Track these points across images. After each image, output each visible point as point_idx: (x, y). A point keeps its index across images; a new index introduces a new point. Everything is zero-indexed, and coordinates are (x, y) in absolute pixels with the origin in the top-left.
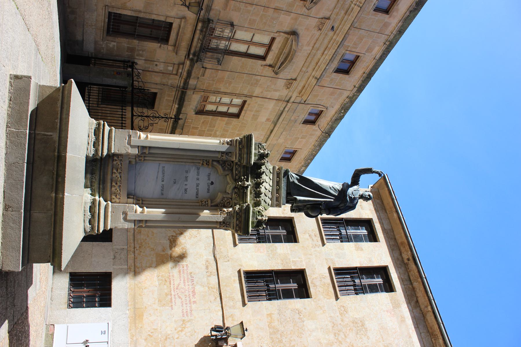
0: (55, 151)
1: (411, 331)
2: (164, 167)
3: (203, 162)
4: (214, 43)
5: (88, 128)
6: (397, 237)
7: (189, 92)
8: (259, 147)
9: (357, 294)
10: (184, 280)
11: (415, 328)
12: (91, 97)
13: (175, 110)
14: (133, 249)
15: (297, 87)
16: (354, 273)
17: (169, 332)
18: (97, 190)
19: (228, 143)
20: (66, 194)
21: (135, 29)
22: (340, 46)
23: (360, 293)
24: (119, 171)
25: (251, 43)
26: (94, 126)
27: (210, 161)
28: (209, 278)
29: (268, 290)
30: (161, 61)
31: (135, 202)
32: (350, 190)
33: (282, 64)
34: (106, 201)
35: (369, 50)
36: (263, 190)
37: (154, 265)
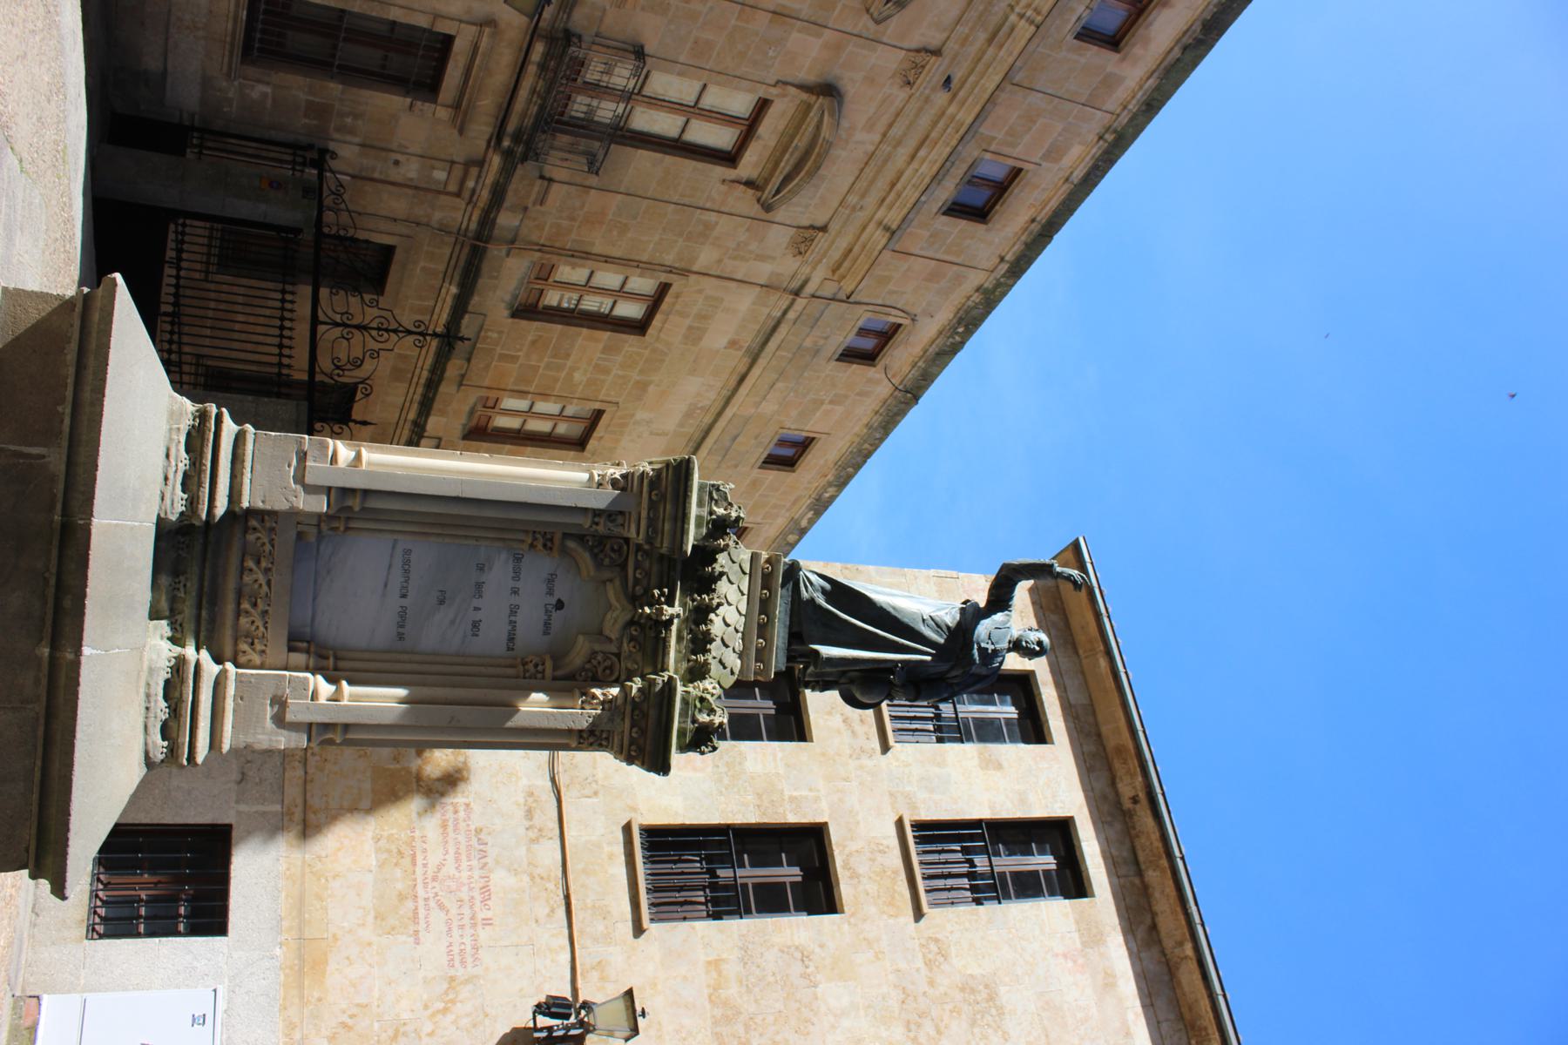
0: (52, 508)
1: (1131, 1016)
2: (408, 552)
4: (580, 105)
5: (165, 427)
6: (1104, 730)
7: (495, 251)
8: (711, 498)
9: (978, 902)
11: (1144, 1006)
12: (185, 247)
13: (449, 301)
15: (826, 252)
16: (972, 838)
17: (405, 1016)
18: (190, 626)
19: (614, 483)
20: (86, 651)
21: (335, 47)
22: (968, 137)
23: (986, 899)
24: (264, 564)
25: (694, 110)
26: (186, 423)
27: (558, 538)
28: (535, 846)
29: (714, 887)
31: (311, 664)
32: (984, 628)
33: (788, 179)
34: (218, 660)
35: (1054, 154)
36: (716, 627)
37: (366, 803)
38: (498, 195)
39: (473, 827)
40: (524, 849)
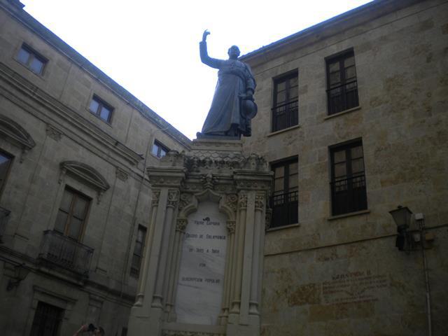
2: (183, 279)
10: (342, 286)
38: (101, 288)
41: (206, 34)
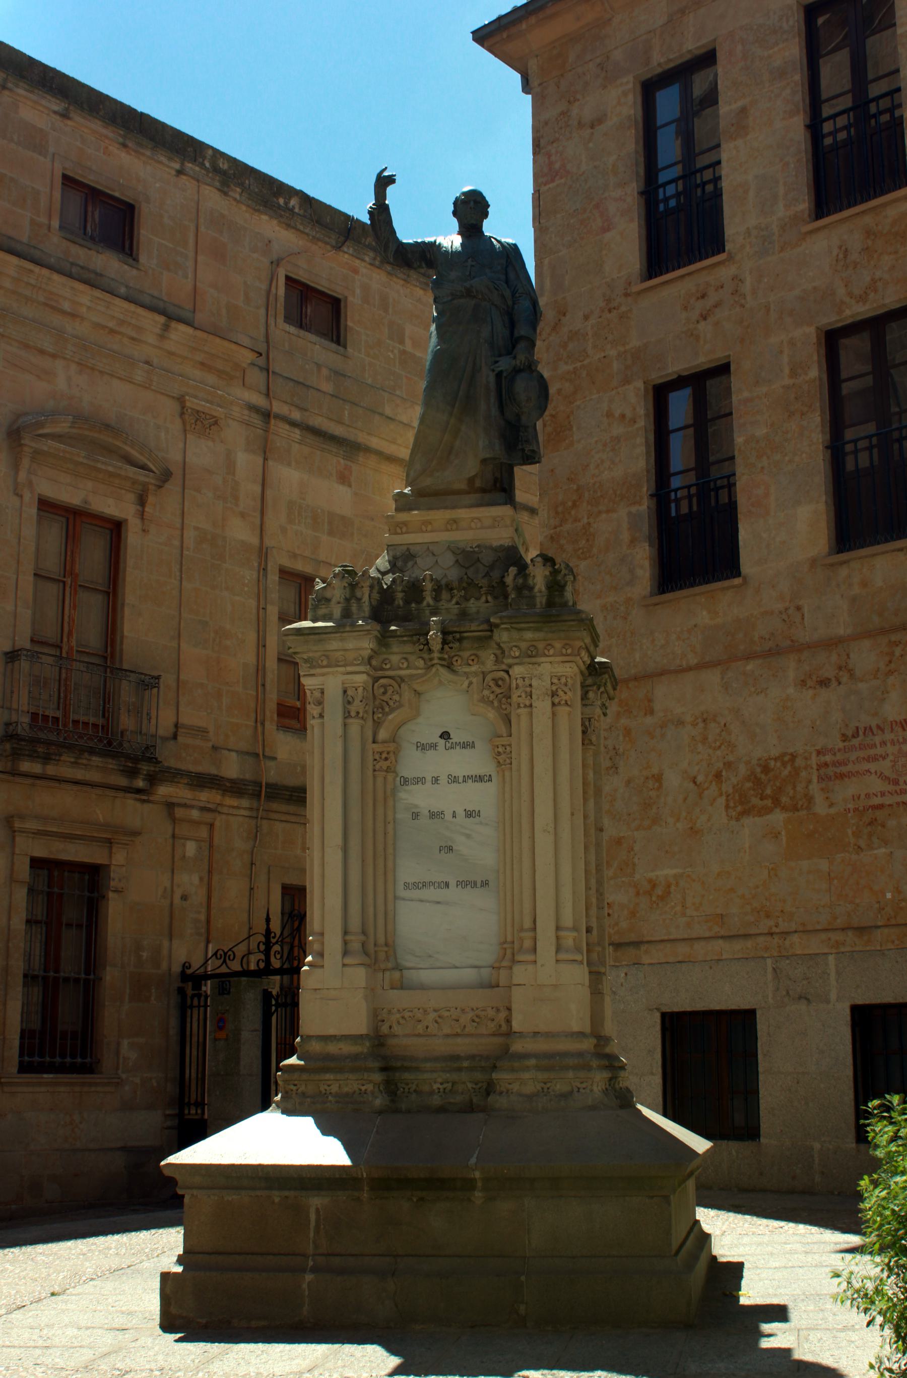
2: (407, 886)
3: (381, 770)
10: (868, 759)
14: (776, 939)
21: (66, 980)
30: (168, 885)
38: (202, 781)
39: (841, 745)
40: (860, 685)
41: (383, 182)
